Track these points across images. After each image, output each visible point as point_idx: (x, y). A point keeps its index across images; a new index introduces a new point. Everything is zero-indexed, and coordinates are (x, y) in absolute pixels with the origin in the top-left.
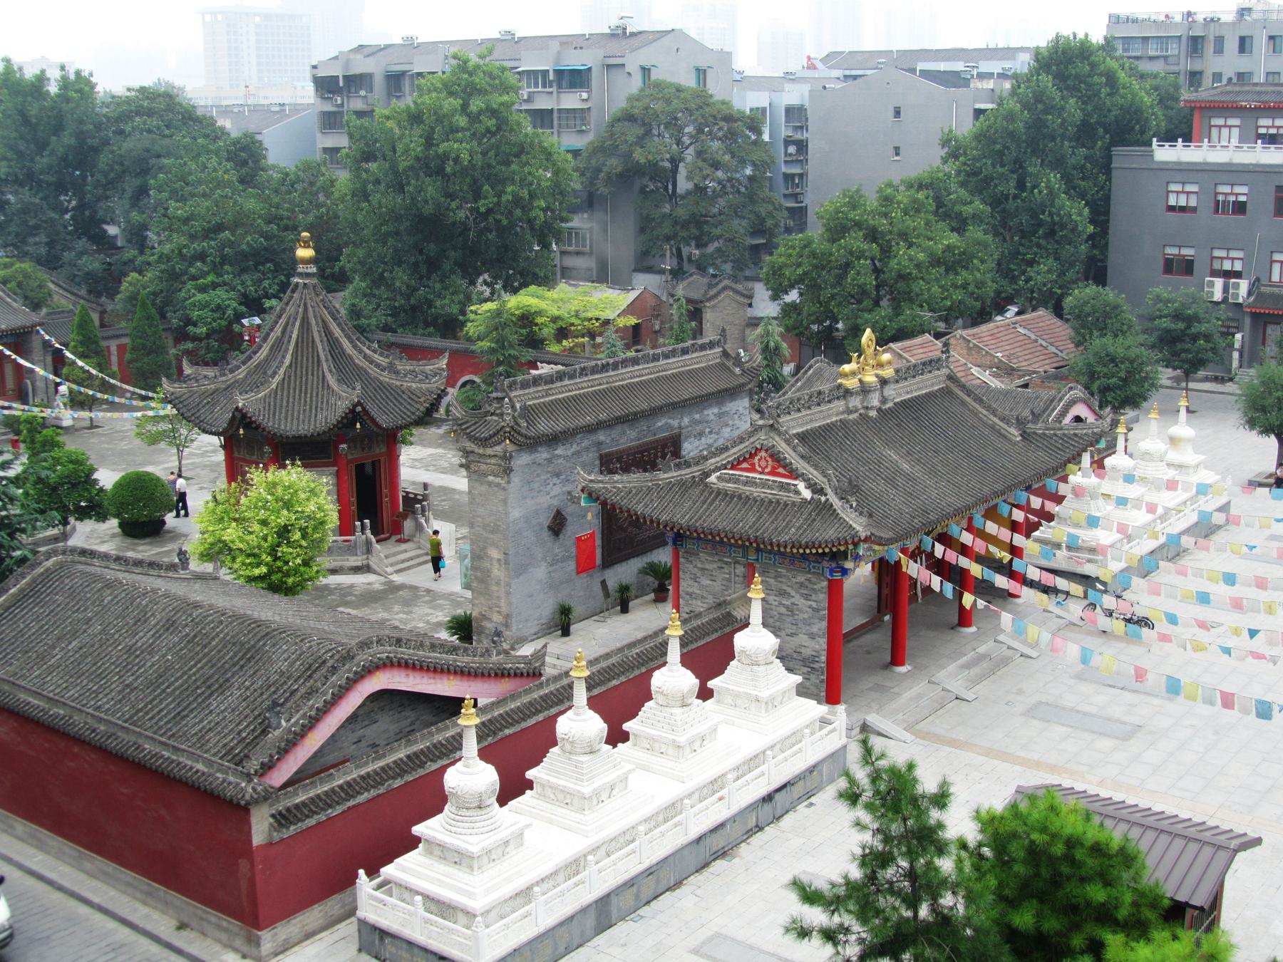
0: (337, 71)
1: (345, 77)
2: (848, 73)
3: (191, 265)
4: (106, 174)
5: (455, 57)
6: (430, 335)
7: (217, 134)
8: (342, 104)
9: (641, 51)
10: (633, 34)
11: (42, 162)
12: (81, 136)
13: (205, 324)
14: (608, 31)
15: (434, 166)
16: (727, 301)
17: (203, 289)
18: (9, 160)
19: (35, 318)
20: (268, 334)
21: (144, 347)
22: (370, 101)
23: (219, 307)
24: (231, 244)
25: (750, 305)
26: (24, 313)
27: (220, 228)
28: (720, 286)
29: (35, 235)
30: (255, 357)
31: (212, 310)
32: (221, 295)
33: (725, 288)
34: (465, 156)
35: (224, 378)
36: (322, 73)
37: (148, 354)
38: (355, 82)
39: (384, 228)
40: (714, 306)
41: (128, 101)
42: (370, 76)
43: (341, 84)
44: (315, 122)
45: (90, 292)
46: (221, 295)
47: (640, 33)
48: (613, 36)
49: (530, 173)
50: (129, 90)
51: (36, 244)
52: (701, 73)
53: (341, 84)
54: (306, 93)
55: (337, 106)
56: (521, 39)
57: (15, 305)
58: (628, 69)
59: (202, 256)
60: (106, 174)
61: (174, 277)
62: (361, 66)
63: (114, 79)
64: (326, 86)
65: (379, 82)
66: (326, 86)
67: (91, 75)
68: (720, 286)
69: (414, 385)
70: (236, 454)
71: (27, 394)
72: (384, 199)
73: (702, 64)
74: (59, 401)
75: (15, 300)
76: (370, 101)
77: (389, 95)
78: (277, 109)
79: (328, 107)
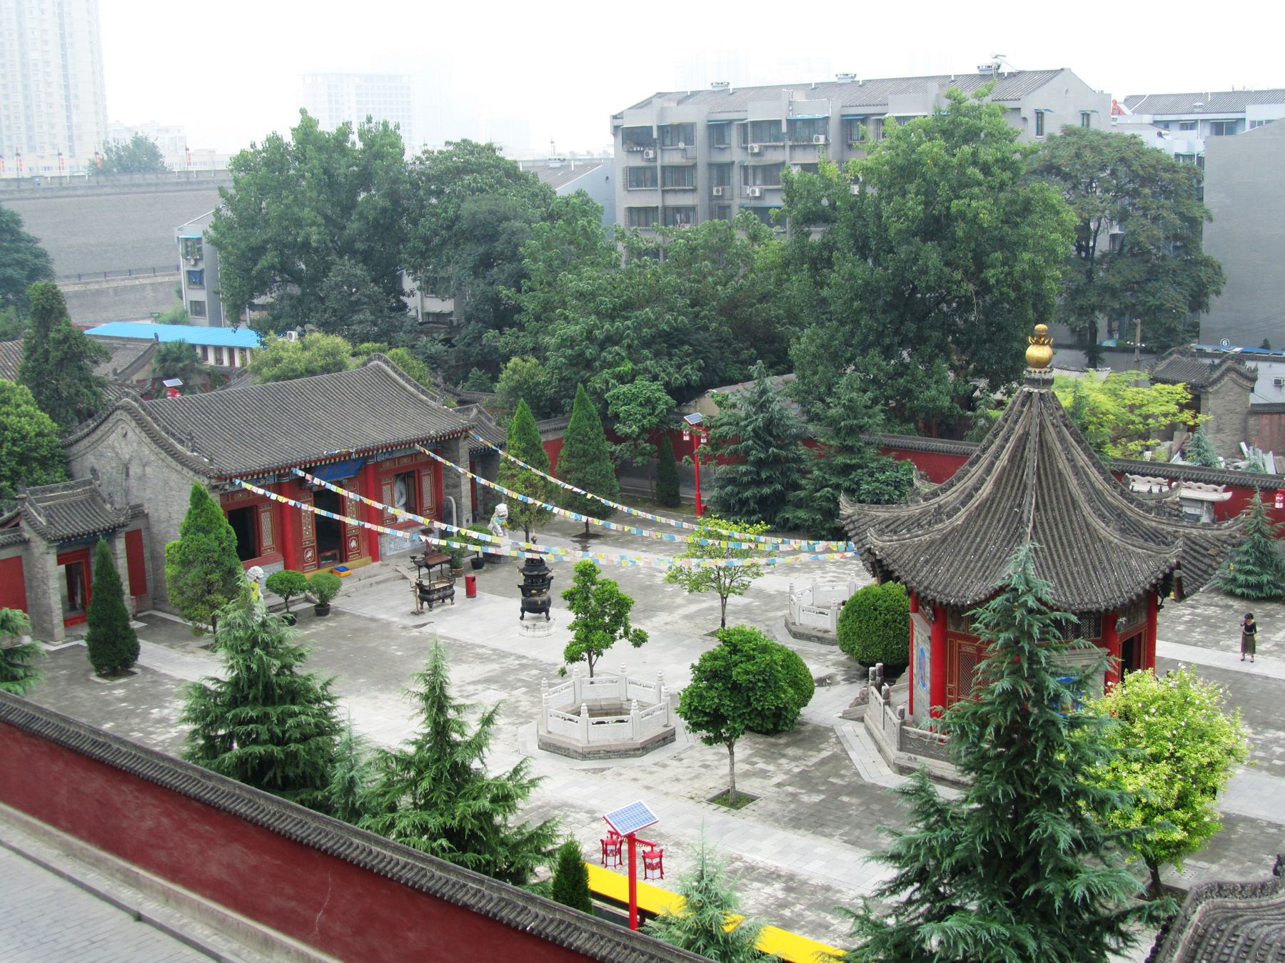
0: (648, 120)
1: (661, 128)
2: (1159, 118)
3: (602, 348)
4: (427, 241)
5: (949, 97)
6: (909, 433)
7: (544, 195)
8: (655, 159)
9: (1035, 93)
10: (1012, 75)
11: (354, 226)
12: (393, 196)
13: (635, 421)
14: (977, 72)
15: (934, 227)
16: (1231, 384)
17: (621, 379)
18: (319, 226)
19: (463, 421)
20: (993, 464)
21: (585, 453)
22: (689, 154)
23: (648, 400)
24: (647, 322)
25: (1252, 390)
26: (448, 414)
27: (628, 306)
28: (1224, 367)
29: (358, 311)
30: (977, 496)
31: (641, 405)
32: (643, 386)
33: (1229, 370)
34: (984, 217)
35: (940, 526)
36: (628, 123)
37: (591, 461)
38: (674, 133)
39: (856, 304)
40: (1217, 392)
41: (448, 156)
42: (691, 126)
43: (655, 135)
44: (619, 180)
45: (446, 380)
46: (643, 386)
47: (1020, 73)
48: (983, 77)
49: (1042, 237)
50: (448, 143)
51: (361, 322)
52: (1086, 116)
53: (655, 135)
54: (604, 144)
55: (649, 160)
56: (866, 82)
57: (433, 403)
58: (1024, 113)
59: (610, 340)
60: (427, 241)
61: (583, 363)
62: (676, 116)
63: (423, 138)
64: (633, 138)
65: (700, 134)
66: (633, 138)
67: (397, 127)
68: (1224, 367)
69: (1195, 532)
70: (951, 629)
71: (450, 514)
72: (850, 270)
73: (1087, 108)
74: (495, 522)
75: (433, 399)
76: (689, 154)
77: (711, 146)
78: (558, 165)
79: (637, 162)
